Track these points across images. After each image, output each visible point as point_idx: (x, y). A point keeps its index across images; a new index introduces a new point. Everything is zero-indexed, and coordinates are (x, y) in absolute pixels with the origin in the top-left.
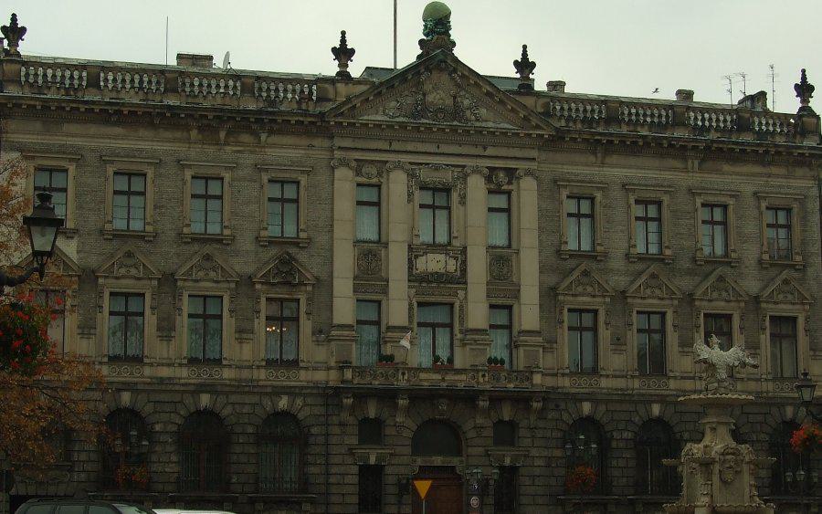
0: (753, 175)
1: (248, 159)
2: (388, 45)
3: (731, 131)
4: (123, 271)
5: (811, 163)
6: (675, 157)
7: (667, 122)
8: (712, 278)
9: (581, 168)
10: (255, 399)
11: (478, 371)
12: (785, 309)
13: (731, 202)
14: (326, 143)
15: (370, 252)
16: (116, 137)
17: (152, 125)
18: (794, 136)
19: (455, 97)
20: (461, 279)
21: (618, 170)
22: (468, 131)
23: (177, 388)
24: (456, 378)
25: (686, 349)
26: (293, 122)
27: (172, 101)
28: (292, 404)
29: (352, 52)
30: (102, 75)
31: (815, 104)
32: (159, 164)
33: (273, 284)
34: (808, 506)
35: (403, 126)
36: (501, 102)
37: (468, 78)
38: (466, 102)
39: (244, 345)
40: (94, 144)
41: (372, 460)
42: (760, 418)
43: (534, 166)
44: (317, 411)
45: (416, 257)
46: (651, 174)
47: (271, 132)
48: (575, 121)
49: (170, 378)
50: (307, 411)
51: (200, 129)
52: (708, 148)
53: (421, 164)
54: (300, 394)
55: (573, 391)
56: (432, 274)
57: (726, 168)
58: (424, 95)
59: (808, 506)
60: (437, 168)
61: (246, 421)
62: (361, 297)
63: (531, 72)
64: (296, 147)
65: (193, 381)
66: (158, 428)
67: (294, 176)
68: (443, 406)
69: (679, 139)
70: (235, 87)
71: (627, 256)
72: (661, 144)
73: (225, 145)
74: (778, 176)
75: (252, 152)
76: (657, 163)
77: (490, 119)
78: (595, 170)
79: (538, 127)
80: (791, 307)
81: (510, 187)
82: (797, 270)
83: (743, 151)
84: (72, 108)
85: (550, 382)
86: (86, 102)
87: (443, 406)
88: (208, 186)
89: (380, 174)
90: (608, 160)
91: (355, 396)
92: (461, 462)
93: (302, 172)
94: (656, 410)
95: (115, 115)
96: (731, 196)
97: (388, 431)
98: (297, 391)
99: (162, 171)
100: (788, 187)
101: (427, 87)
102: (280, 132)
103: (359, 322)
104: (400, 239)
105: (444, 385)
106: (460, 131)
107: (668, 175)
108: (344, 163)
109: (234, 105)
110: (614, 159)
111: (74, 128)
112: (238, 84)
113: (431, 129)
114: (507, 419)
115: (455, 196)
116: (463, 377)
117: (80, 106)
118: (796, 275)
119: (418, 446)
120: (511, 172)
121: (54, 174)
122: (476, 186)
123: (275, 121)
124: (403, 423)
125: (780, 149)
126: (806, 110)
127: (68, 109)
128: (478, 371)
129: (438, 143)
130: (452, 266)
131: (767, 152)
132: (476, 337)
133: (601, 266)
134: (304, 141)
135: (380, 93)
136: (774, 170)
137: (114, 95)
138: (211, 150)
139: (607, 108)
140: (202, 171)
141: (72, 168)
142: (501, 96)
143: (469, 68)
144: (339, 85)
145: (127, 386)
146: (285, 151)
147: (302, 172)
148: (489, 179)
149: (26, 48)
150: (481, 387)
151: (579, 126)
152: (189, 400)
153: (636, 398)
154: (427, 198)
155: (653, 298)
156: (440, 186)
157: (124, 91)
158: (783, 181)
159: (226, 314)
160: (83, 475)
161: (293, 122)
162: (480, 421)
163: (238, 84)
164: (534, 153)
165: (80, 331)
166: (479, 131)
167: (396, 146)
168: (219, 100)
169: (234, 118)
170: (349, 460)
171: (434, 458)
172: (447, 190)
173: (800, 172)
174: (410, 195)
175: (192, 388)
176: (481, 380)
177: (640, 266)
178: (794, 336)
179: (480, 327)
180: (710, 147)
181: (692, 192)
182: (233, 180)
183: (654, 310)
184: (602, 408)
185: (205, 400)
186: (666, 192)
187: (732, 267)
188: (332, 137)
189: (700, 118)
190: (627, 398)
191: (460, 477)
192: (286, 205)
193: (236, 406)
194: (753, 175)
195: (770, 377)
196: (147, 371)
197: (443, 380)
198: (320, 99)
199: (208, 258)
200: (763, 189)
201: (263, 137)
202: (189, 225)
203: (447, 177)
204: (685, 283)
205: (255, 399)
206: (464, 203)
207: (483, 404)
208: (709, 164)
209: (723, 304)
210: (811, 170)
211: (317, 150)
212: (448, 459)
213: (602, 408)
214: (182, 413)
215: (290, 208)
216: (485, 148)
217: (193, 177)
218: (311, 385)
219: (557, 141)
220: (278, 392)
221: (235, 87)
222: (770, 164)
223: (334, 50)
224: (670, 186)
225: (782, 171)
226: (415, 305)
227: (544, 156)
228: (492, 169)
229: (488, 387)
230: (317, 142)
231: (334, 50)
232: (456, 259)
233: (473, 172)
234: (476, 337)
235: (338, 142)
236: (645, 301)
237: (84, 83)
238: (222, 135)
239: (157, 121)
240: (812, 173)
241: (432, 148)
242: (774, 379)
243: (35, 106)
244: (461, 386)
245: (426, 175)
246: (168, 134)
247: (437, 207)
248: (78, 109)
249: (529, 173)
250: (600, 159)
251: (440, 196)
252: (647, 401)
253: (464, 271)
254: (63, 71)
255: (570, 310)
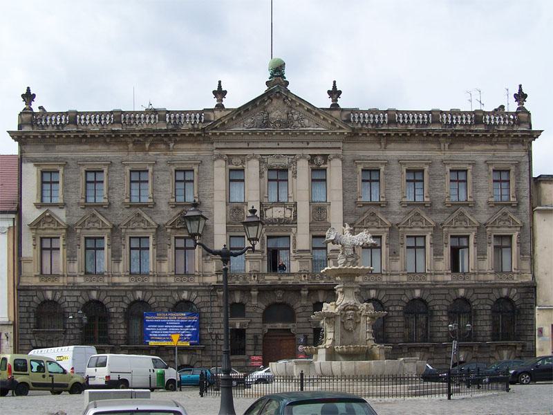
0: (486, 150)
1: (162, 158)
2: (245, 88)
3: (471, 125)
4: (46, 226)
5: (523, 141)
6: (432, 142)
7: (428, 122)
8: (456, 214)
9: (371, 152)
10: (168, 294)
11: (301, 274)
12: (504, 231)
13: (470, 168)
14: (210, 146)
15: (237, 208)
16: (85, 151)
17: (106, 143)
18: (513, 126)
19: (288, 114)
20: (294, 222)
21: (395, 152)
22: (296, 133)
23: (123, 288)
24: (287, 278)
25: (438, 257)
26: (218, 134)
27: (117, 128)
28: (190, 296)
29: (340, 92)
30: (78, 116)
31: (527, 105)
32: (66, 165)
33: (178, 229)
34: (515, 347)
35: (254, 133)
36: (316, 114)
37: (295, 102)
38: (295, 117)
39: (162, 264)
40: (74, 155)
41: (238, 326)
42: (486, 296)
43: (339, 152)
44: (205, 299)
45: (266, 210)
46: (410, 153)
47: (176, 142)
48: (367, 125)
49: (119, 283)
50: (199, 300)
51: (134, 143)
52: (453, 135)
53: (268, 155)
54: (195, 290)
55: (364, 283)
56: (275, 219)
57: (467, 147)
58: (268, 114)
59: (515, 347)
60: (278, 157)
61: (164, 305)
62: (315, 234)
63: (338, 96)
64: (190, 150)
65: (132, 284)
66: (113, 310)
67: (464, 166)
68: (279, 294)
69: (480, 131)
70: (155, 118)
71: (401, 203)
72: (422, 135)
73: (148, 151)
74: (500, 150)
75: (165, 155)
76: (421, 146)
77: (310, 125)
78: (380, 153)
79: (340, 128)
80: (507, 229)
81: (326, 166)
82: (513, 207)
83: (477, 136)
84: (220, 133)
85: (433, 278)
86: (65, 132)
87: (279, 294)
88: (459, 175)
89: (243, 163)
90: (389, 146)
91: (259, 290)
92: (294, 326)
93: (195, 164)
94: (418, 293)
95: (84, 138)
96: (469, 164)
97: (247, 309)
98: (193, 288)
99: (112, 168)
100: (508, 157)
101: (270, 109)
102: (182, 142)
103: (314, 248)
104: (254, 200)
105: (280, 282)
106: (290, 133)
107: (425, 153)
108: (220, 157)
109: (154, 128)
110: (392, 146)
111: (62, 147)
112: (157, 117)
113: (272, 133)
114: (237, 301)
115: (290, 172)
116: (292, 278)
117: (79, 134)
118: (512, 210)
119: (267, 316)
120: (325, 157)
121: (372, 173)
122: (303, 167)
123: (509, 135)
124: (256, 306)
125: (501, 133)
126: (522, 110)
127: (56, 136)
128: (301, 274)
129: (278, 142)
130: (288, 214)
131: (493, 136)
132: (302, 254)
133: (384, 210)
134: (197, 146)
135: (239, 115)
136: (498, 147)
137: (84, 127)
138: (141, 155)
139: (432, 116)
140: (136, 167)
141: (61, 170)
142: (316, 111)
143: (258, 98)
144: (216, 112)
145: (93, 288)
146: (185, 153)
147: (195, 164)
148: (311, 161)
149: (343, 103)
150: (302, 283)
151: (370, 127)
152: (130, 295)
153: (404, 287)
154: (274, 175)
155: (418, 227)
156: (281, 168)
157: (150, 125)
158: (504, 154)
159: (428, 245)
160: (72, 336)
161: (218, 134)
162: (304, 303)
163: (157, 117)
164: (340, 145)
165: (68, 259)
166: (302, 133)
167: (282, 145)
168: (145, 127)
169: (152, 135)
170: (307, 325)
171: (277, 324)
172: (285, 170)
173: (515, 147)
174: (261, 173)
175: (131, 288)
176: (303, 279)
177: (409, 209)
178: (510, 247)
179: (305, 249)
180: (454, 135)
181: (444, 163)
182: (154, 171)
183: (420, 234)
184: (383, 294)
185: (139, 295)
186: (426, 164)
187: (426, 207)
188: (212, 143)
189: (450, 118)
190: (399, 287)
191: (293, 335)
192: (460, 184)
193: (158, 298)
194: (486, 150)
195: (493, 271)
196: (106, 280)
197: (280, 279)
198: (205, 121)
199: (505, 214)
200: (491, 159)
201: (172, 145)
202: (360, 197)
203: (285, 162)
204: (440, 218)
205: (168, 294)
206: (296, 177)
207: (304, 293)
208: (455, 146)
209: (463, 229)
210: (523, 145)
211: (204, 151)
212: (285, 325)
213: (383, 294)
214: (126, 302)
215: (462, 185)
216: (308, 144)
217: (363, 170)
218: (202, 285)
219: (354, 136)
220: (181, 289)
221: (155, 118)
222: (495, 143)
223: (329, 92)
224: (429, 160)
225: (504, 147)
226: (266, 238)
227: (346, 146)
228: (313, 156)
229: (307, 283)
230: (204, 146)
231: (329, 92)
232: (291, 210)
233: (301, 158)
234: (302, 254)
235: (215, 145)
236: (500, 229)
237: (386, 120)
238: (147, 146)
239: (108, 140)
240: (524, 148)
241: (274, 145)
242: (495, 273)
243: (37, 136)
244: (290, 283)
245: (272, 162)
246: (116, 148)
247: (280, 180)
248: (61, 136)
249: (337, 156)
250: (383, 146)
251: (279, 175)
252: (499, 287)
253: (295, 217)
254: (423, 115)
255: (451, 236)
